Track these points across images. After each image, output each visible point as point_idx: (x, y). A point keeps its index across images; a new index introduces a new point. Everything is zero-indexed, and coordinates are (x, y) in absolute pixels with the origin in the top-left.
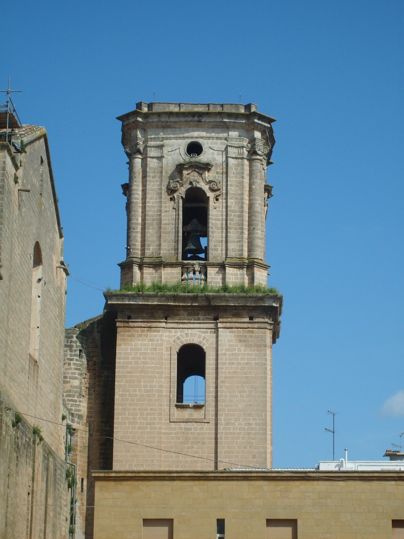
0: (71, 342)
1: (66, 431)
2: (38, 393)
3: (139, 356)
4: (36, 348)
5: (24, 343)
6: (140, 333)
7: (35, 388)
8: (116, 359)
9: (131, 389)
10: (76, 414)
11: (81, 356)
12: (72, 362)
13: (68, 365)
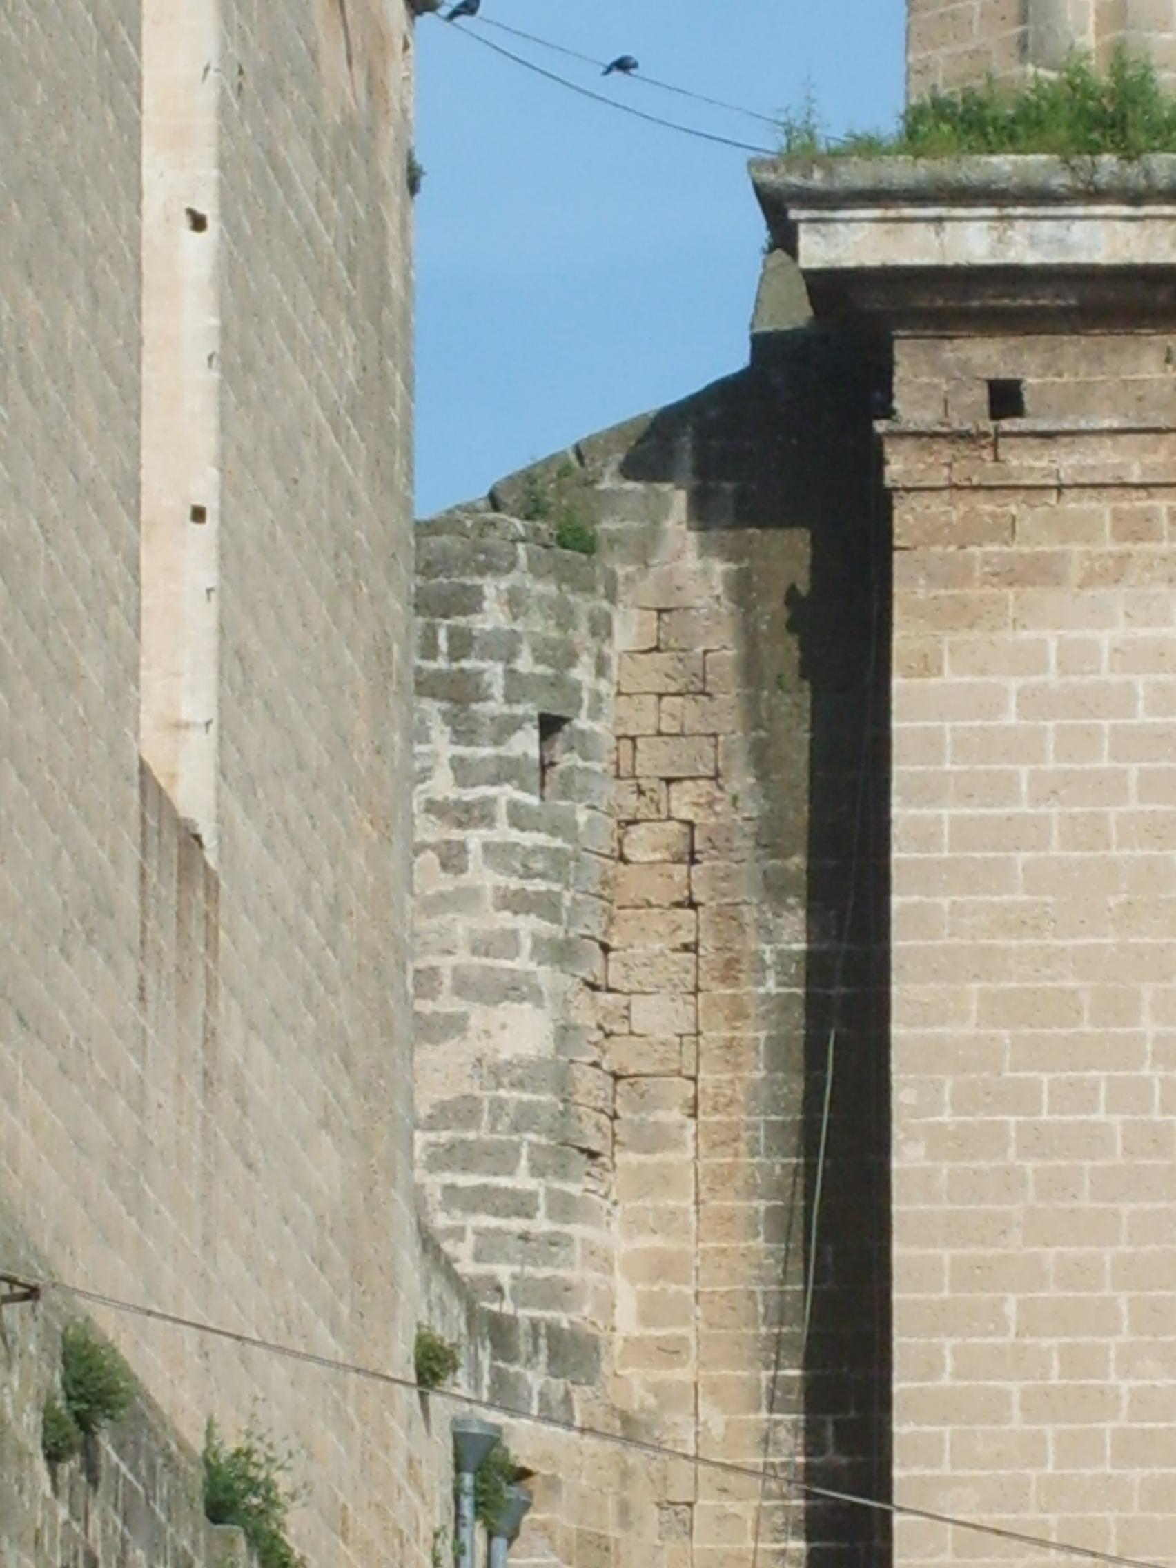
0: (462, 644)
1: (448, 1490)
2: (225, 1142)
3: (1105, 764)
4: (186, 713)
5: (93, 668)
6: (1112, 547)
7: (193, 1085)
8: (895, 800)
9: (1045, 1078)
10: (534, 1324)
11: (552, 774)
12: (475, 838)
13: (444, 866)
